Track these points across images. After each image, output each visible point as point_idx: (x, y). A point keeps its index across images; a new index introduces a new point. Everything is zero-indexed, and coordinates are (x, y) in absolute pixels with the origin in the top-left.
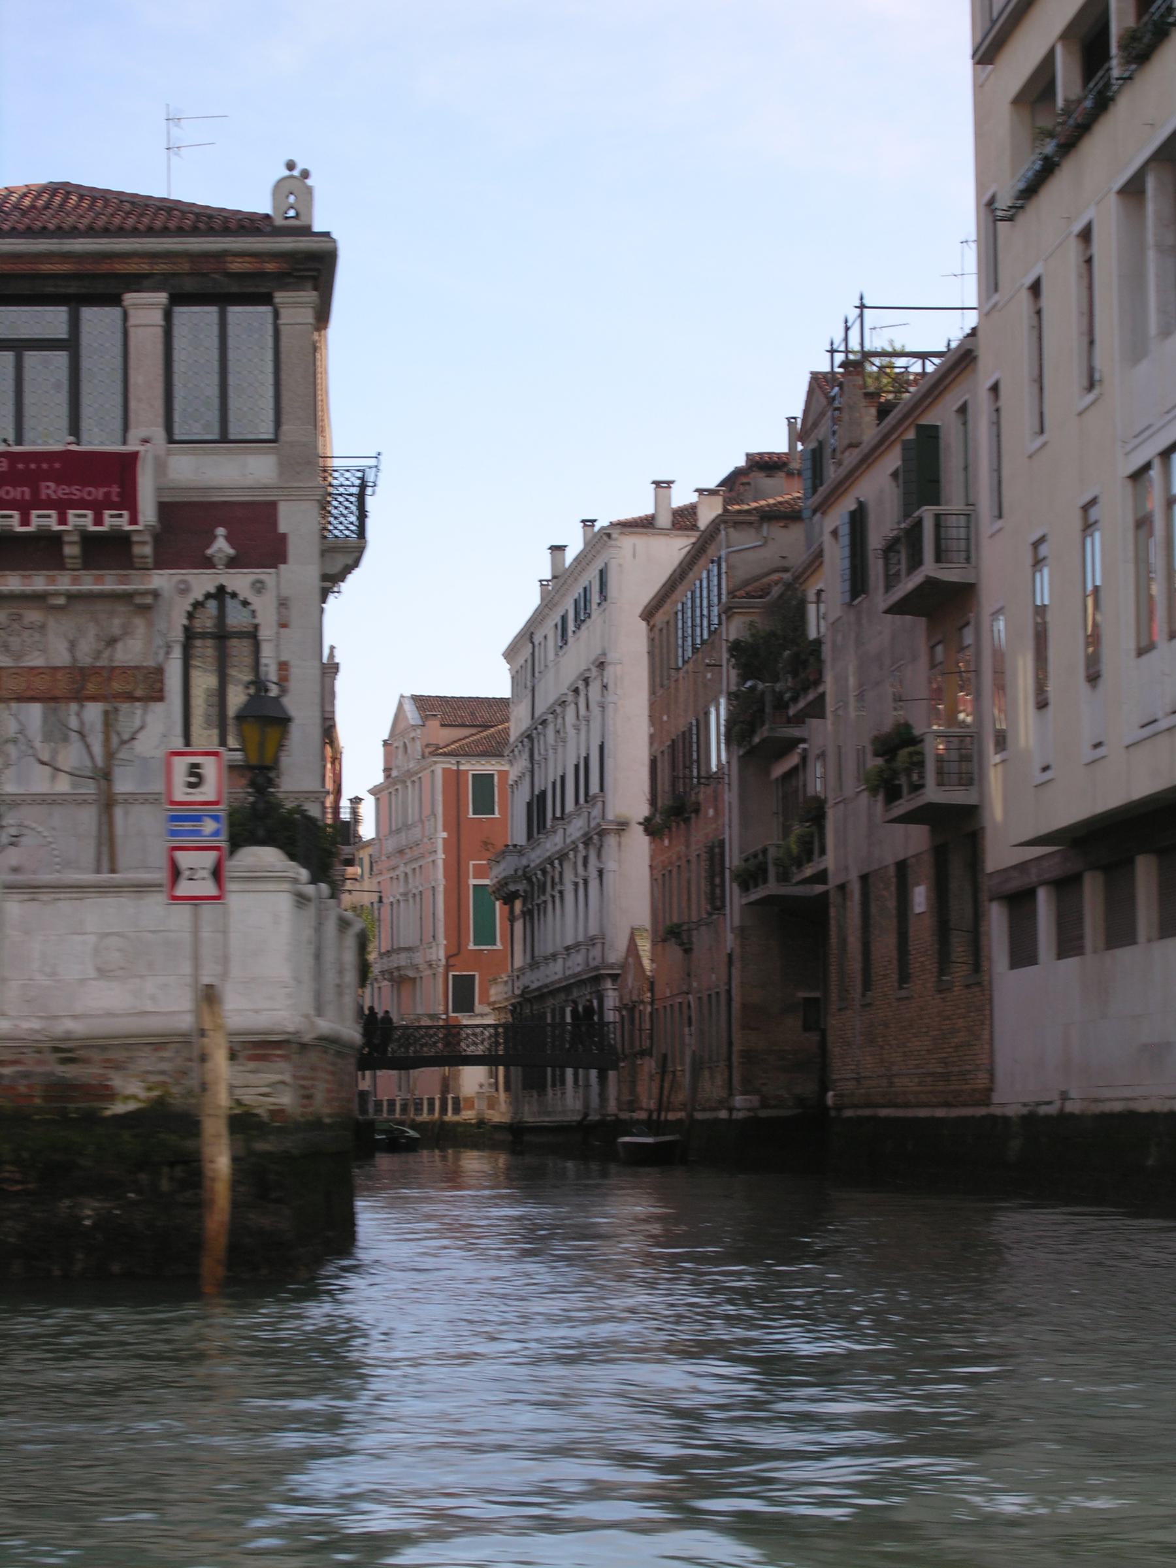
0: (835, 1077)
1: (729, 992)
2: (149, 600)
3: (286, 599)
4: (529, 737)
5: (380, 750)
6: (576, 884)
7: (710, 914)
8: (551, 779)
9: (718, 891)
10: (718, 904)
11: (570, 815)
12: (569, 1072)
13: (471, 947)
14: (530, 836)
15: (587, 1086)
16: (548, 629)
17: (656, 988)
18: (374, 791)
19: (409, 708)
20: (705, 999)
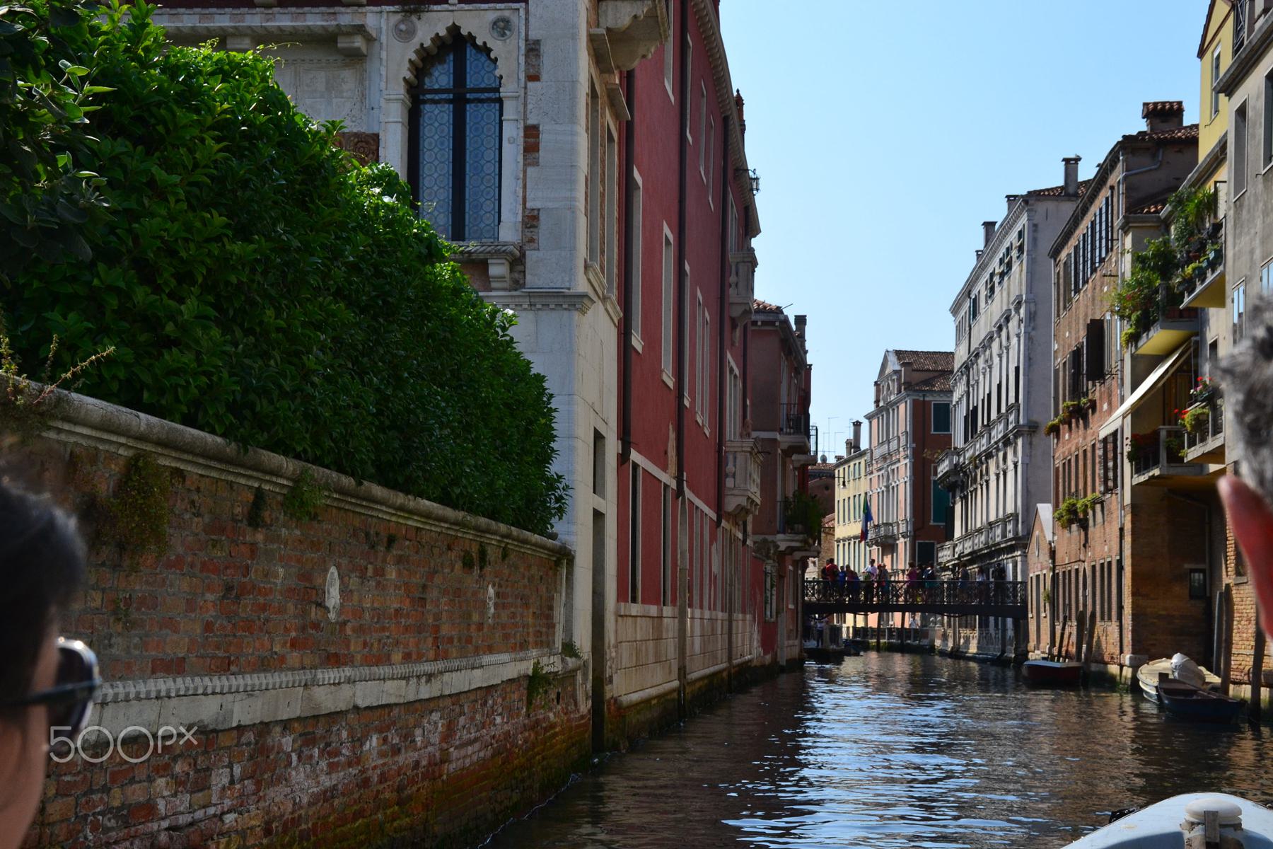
0: (732, 300)
1: (1120, 562)
2: (359, 42)
3: (537, 42)
4: (967, 367)
5: (873, 389)
6: (998, 475)
7: (1104, 494)
8: (981, 397)
9: (1111, 474)
10: (1110, 484)
11: (994, 422)
12: (992, 619)
13: (932, 523)
14: (966, 440)
15: (1004, 630)
16: (981, 288)
17: (1058, 556)
18: (870, 417)
19: (894, 365)
20: (1098, 568)
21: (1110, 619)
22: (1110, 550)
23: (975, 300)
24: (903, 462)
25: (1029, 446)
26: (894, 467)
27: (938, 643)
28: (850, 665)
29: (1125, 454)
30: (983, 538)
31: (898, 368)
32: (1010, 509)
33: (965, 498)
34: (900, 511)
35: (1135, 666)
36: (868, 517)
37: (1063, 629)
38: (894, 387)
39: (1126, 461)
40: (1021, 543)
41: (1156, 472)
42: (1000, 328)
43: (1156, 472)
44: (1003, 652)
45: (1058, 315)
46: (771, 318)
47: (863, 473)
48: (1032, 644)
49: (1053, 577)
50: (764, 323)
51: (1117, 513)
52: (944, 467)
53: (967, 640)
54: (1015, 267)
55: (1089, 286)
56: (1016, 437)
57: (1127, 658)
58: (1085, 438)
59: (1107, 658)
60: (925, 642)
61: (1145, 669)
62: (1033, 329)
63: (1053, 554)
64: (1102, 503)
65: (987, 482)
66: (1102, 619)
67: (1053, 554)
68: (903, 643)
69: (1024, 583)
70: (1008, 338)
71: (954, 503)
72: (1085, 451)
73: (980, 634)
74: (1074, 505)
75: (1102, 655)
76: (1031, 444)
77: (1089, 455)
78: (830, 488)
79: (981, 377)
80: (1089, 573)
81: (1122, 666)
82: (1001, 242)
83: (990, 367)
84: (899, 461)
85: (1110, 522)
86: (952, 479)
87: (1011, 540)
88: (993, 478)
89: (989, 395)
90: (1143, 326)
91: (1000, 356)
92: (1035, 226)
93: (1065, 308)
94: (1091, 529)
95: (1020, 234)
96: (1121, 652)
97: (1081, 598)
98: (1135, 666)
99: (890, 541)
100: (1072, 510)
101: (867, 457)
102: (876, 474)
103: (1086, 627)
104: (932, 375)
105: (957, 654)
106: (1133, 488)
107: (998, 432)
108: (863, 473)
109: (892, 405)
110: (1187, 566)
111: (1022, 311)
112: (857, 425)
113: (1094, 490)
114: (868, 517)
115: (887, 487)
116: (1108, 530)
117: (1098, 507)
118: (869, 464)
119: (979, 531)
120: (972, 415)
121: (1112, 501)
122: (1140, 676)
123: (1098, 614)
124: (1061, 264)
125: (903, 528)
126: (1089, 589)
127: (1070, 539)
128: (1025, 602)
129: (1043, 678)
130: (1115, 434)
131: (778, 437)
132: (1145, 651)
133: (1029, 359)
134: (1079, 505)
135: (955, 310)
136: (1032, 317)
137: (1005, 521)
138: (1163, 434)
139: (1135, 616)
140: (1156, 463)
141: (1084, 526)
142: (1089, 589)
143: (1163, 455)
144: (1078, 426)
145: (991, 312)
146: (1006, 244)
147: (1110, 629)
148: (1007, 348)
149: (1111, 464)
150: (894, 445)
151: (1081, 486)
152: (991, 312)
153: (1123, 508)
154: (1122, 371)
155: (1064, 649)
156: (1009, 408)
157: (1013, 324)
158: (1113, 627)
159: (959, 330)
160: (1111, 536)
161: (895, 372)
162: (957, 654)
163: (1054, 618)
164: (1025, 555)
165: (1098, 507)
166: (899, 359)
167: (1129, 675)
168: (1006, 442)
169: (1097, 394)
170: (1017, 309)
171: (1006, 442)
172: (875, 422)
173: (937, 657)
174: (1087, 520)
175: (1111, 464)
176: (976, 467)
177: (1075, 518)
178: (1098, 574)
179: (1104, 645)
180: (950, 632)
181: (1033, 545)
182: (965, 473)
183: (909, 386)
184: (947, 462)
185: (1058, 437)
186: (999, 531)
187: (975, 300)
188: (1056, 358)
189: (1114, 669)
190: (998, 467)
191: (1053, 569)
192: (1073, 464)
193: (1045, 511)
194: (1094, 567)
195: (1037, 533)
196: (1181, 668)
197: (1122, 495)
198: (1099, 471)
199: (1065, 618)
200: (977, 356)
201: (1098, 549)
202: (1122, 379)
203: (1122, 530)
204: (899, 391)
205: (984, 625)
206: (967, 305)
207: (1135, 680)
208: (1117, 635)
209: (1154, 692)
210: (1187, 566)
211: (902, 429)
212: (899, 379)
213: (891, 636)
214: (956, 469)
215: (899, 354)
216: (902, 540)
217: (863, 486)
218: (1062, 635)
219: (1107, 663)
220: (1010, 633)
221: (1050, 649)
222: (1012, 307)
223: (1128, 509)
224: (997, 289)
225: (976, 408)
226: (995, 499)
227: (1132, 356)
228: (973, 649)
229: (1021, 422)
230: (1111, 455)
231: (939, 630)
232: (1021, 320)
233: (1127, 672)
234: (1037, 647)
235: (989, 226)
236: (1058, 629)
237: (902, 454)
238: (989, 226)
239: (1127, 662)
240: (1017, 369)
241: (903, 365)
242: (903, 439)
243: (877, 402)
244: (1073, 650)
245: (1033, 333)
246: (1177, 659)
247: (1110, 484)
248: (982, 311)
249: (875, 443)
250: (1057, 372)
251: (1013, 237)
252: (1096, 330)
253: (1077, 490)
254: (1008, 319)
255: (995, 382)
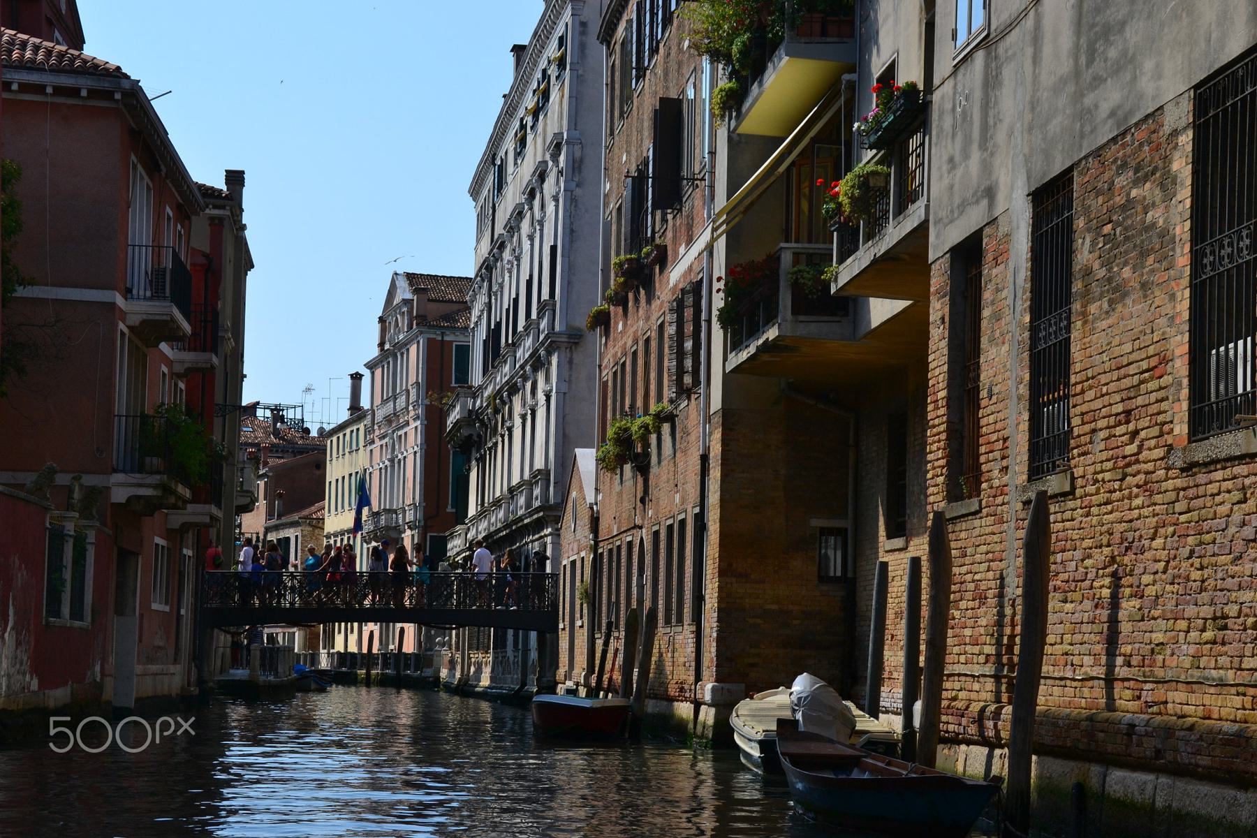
1: (700, 520)
5: (376, 328)
6: (524, 417)
8: (505, 306)
9: (688, 363)
10: (688, 380)
12: (510, 632)
16: (509, 144)
18: (371, 366)
19: (404, 292)
21: (680, 621)
22: (683, 500)
23: (501, 167)
24: (413, 425)
25: (568, 366)
26: (401, 432)
27: (444, 673)
28: (332, 705)
29: (715, 313)
30: (501, 514)
31: (409, 296)
32: (539, 464)
33: (481, 460)
34: (408, 492)
35: (724, 706)
36: (363, 500)
37: (606, 644)
38: (403, 322)
39: (716, 326)
40: (551, 514)
41: (772, 333)
42: (532, 195)
43: (772, 333)
44: (524, 684)
45: (612, 134)
46: (105, 85)
47: (361, 443)
48: (562, 671)
49: (594, 559)
50: (93, 93)
51: (696, 433)
52: (454, 416)
53: (479, 671)
54: (554, 96)
55: (659, 57)
56: (549, 354)
57: (707, 689)
58: (648, 319)
59: (673, 691)
60: (428, 672)
61: (744, 707)
62: (578, 185)
63: (595, 522)
64: (671, 418)
65: (510, 430)
66: (668, 621)
67: (595, 522)
68: (398, 673)
69: (555, 576)
70: (543, 207)
71: (469, 470)
72: (647, 341)
73: (495, 658)
74: (626, 430)
75: (665, 685)
76: (571, 362)
77: (654, 344)
78: (320, 466)
79: (507, 278)
80: (648, 546)
81: (697, 705)
82: (535, 64)
83: (518, 259)
84: (407, 424)
85: (685, 451)
86: (465, 432)
87: (537, 510)
88: (518, 421)
89: (516, 301)
90: (748, 70)
91: (531, 238)
92: (583, 24)
93: (621, 116)
94: (654, 470)
95: (562, 40)
96: (698, 678)
97: (635, 590)
98: (724, 706)
99: (393, 535)
100: (624, 440)
101: (368, 421)
102: (378, 443)
103: (640, 631)
104: (455, 307)
105: (465, 689)
106: (726, 376)
107: (523, 353)
108: (361, 443)
109: (402, 347)
110: (816, 523)
111: (562, 158)
112: (356, 378)
113: (660, 398)
114: (363, 500)
115: (392, 461)
116: (681, 465)
117: (666, 428)
118: (369, 431)
119: (497, 503)
120: (494, 334)
121: (690, 412)
122: (735, 721)
123: (661, 615)
124: (618, 48)
125: (410, 516)
126: (648, 572)
127: (620, 494)
128: (555, 606)
129: (566, 728)
130: (696, 288)
131: (120, 301)
132: (742, 676)
133: (571, 232)
134: (634, 428)
135: (475, 191)
136: (576, 166)
137: (527, 485)
138: (786, 259)
139: (723, 613)
140: (770, 320)
141: (643, 468)
142: (648, 572)
143: (785, 299)
144: (637, 300)
145: (520, 175)
146: (543, 64)
147: (679, 638)
148: (541, 223)
149: (688, 345)
150: (401, 402)
151: (640, 403)
152: (520, 175)
153: (708, 419)
154: (712, 173)
155: (606, 677)
156: (542, 307)
157: (549, 186)
158: (685, 637)
159: (481, 218)
160: (687, 477)
161: (406, 302)
162: (465, 689)
163: (593, 627)
164: (557, 534)
165: (666, 428)
166: (411, 284)
167: (711, 721)
168: (537, 363)
169: (669, 234)
170: (555, 157)
171: (537, 363)
172: (378, 372)
173: (443, 695)
174: (647, 455)
175: (688, 345)
176: (496, 411)
177: (629, 454)
178: (663, 545)
179: (668, 669)
180: (458, 656)
181: (568, 516)
182: (482, 422)
183: (422, 320)
184: (458, 408)
185: (607, 333)
186: (522, 501)
187: (501, 167)
188: (606, 205)
189: (684, 710)
190: (524, 404)
191: (595, 548)
192: (628, 368)
193: (586, 459)
194: (656, 534)
195: (574, 494)
196: (809, 702)
197: (708, 396)
198: (669, 363)
199: (609, 625)
200: (502, 246)
201: (664, 502)
202: (712, 187)
203: (704, 459)
204: (410, 327)
205: (500, 644)
206: (490, 180)
207: (724, 731)
208: (690, 649)
209: (756, 753)
210: (816, 523)
211: (412, 379)
212: (410, 312)
213: (386, 665)
214: (472, 417)
215: (411, 277)
216: (408, 532)
217: (361, 460)
218: (605, 652)
219: (672, 700)
220: (534, 655)
221: (587, 677)
222: (548, 157)
223: (717, 420)
224: (530, 138)
225: (498, 325)
226: (523, 451)
227: (731, 134)
228: (485, 681)
229: (557, 328)
230: (689, 328)
231: (446, 653)
232: (560, 172)
233: (708, 715)
234: (568, 676)
235: (518, 50)
236: (599, 643)
237: (412, 413)
238: (518, 50)
239: (708, 697)
240: (553, 249)
241: (416, 291)
242: (413, 393)
243: (381, 345)
244: (617, 677)
245: (578, 192)
246: (802, 684)
247: (688, 380)
248: (510, 178)
249: (378, 401)
250: (607, 226)
251: (552, 50)
252: (670, 120)
253: (633, 406)
254: (542, 177)
255: (524, 277)
